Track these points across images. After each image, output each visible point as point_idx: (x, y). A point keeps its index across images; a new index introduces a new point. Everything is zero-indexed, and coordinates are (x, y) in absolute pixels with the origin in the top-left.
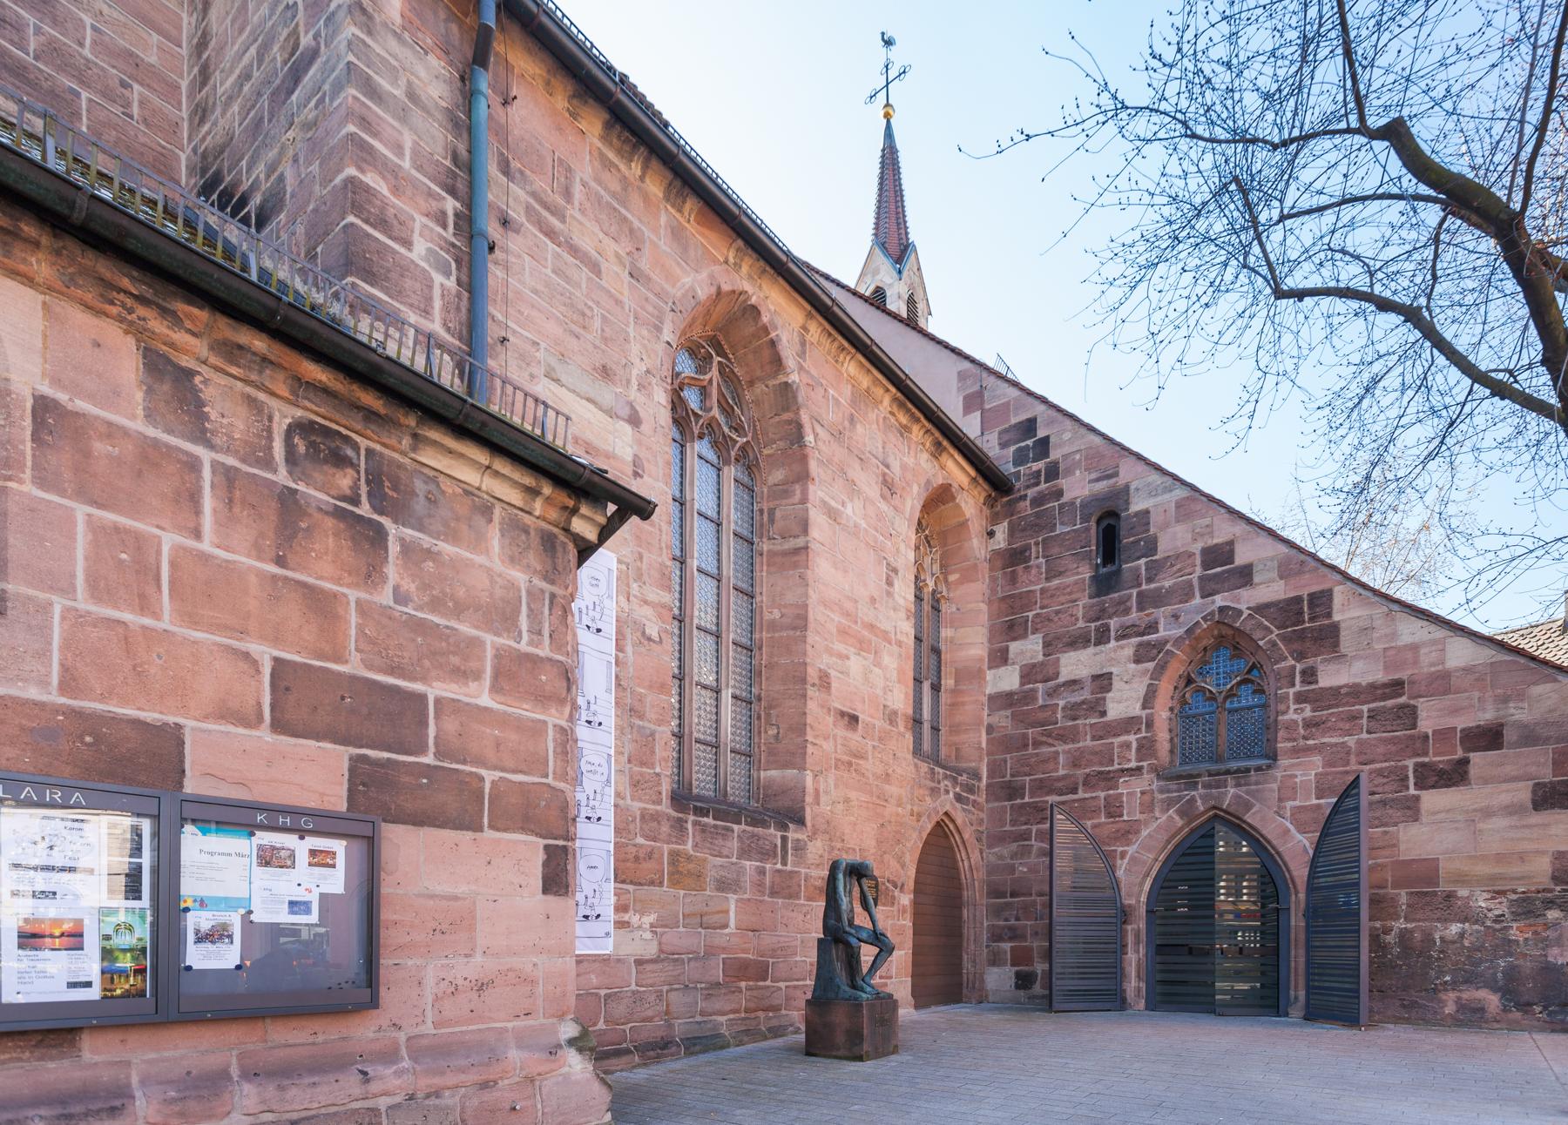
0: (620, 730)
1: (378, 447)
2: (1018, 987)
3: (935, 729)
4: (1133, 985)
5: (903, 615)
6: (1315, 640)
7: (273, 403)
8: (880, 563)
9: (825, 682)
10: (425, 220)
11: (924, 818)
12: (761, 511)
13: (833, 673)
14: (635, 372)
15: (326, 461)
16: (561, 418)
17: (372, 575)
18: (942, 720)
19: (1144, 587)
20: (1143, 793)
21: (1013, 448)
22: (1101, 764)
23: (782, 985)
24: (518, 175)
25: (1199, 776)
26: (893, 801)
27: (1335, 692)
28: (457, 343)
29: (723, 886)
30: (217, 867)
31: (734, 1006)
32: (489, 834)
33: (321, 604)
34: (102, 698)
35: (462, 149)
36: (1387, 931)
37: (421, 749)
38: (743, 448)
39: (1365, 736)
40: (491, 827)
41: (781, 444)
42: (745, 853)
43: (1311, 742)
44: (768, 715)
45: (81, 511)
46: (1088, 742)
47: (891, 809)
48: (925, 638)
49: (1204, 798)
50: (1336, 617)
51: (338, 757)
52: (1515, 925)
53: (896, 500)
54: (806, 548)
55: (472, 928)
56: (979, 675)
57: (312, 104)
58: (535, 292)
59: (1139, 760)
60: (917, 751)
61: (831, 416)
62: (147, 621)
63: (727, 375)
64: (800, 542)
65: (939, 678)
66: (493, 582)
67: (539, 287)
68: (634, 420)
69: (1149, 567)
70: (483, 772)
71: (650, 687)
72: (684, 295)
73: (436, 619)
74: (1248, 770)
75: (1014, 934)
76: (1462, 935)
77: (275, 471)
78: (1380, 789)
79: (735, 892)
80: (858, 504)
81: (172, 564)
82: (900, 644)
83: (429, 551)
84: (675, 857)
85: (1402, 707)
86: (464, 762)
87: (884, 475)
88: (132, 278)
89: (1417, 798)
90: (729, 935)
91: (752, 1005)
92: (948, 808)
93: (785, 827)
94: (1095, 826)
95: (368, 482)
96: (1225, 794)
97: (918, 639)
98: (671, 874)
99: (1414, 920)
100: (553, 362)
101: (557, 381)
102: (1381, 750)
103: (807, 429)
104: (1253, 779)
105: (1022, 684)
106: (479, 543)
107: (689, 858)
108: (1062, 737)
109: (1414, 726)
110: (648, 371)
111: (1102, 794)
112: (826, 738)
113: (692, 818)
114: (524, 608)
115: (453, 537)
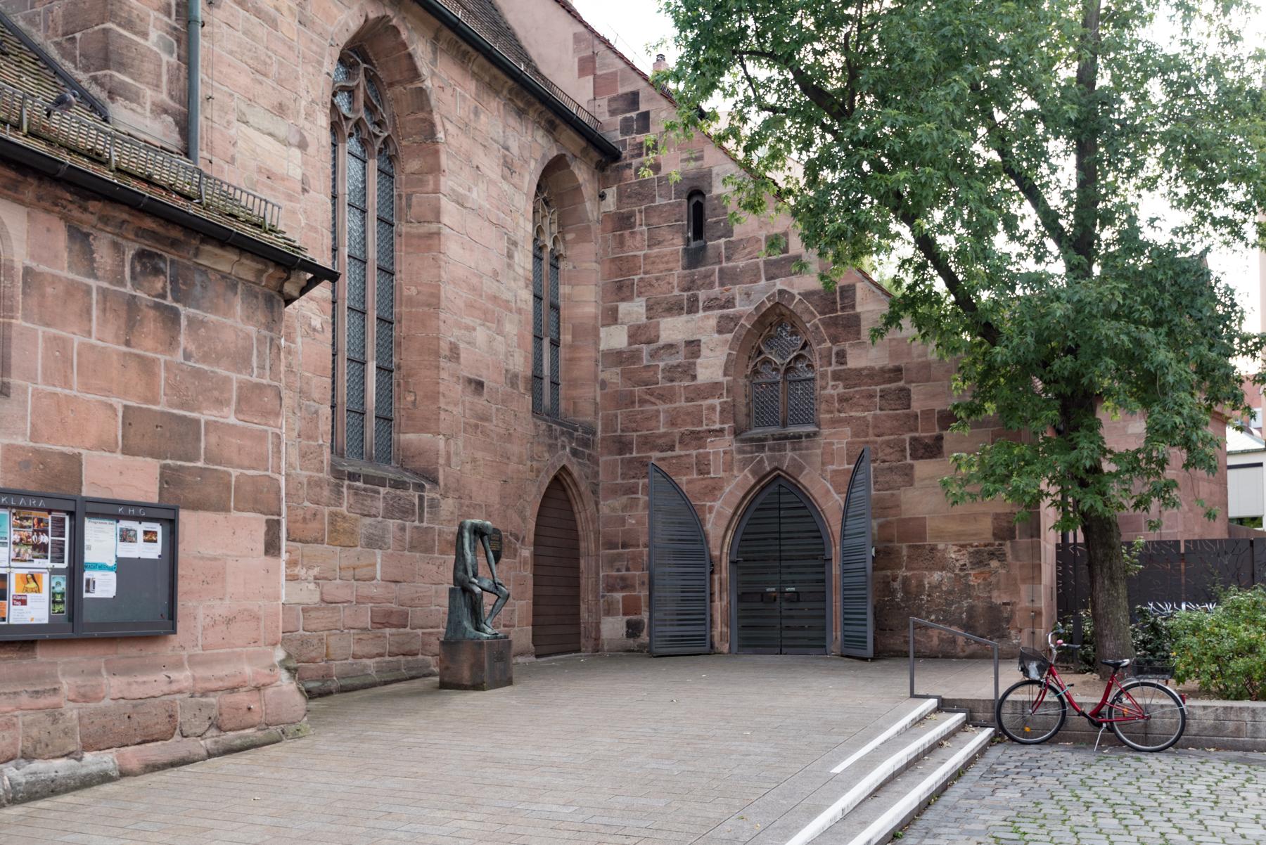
1: (176, 258)
2: (629, 635)
3: (555, 384)
4: (720, 629)
5: (522, 283)
6: (845, 326)
7: (124, 242)
12: (400, 196)
13: (462, 346)
14: (303, 103)
15: (150, 274)
16: (276, 209)
17: (172, 343)
18: (561, 375)
19: (724, 264)
20: (725, 453)
21: (620, 117)
22: (693, 425)
23: (419, 631)
25: (765, 439)
26: (515, 459)
27: (858, 372)
28: (177, 106)
29: (373, 542)
33: (146, 366)
37: (197, 459)
38: (386, 141)
39: (878, 412)
41: (418, 138)
42: (389, 514)
43: (842, 415)
44: (407, 383)
45: (41, 330)
47: (512, 466)
48: (544, 296)
49: (771, 459)
50: (859, 309)
52: (972, 572)
53: (516, 179)
54: (438, 234)
58: (231, 53)
59: (722, 422)
60: (537, 410)
63: (372, 79)
64: (433, 227)
65: (559, 333)
66: (237, 335)
67: (235, 49)
68: (303, 145)
69: (729, 246)
70: (230, 470)
72: (340, 31)
73: (205, 367)
74: (800, 437)
75: (625, 584)
77: (125, 286)
78: (888, 458)
80: (482, 186)
81: (79, 354)
82: (519, 311)
83: (202, 322)
84: (334, 515)
85: (902, 389)
86: (220, 464)
87: (505, 157)
88: (70, 192)
89: (912, 467)
91: (394, 649)
92: (565, 462)
94: (689, 482)
95: (171, 282)
96: (785, 456)
97: (537, 298)
98: (331, 532)
99: (912, 569)
100: (243, 107)
101: (246, 123)
102: (888, 424)
103: (439, 127)
104: (804, 444)
105: (630, 344)
108: (664, 397)
109: (909, 407)
110: (313, 101)
111: (694, 453)
112: (456, 404)
113: (346, 482)
114: (255, 351)
115: (214, 309)
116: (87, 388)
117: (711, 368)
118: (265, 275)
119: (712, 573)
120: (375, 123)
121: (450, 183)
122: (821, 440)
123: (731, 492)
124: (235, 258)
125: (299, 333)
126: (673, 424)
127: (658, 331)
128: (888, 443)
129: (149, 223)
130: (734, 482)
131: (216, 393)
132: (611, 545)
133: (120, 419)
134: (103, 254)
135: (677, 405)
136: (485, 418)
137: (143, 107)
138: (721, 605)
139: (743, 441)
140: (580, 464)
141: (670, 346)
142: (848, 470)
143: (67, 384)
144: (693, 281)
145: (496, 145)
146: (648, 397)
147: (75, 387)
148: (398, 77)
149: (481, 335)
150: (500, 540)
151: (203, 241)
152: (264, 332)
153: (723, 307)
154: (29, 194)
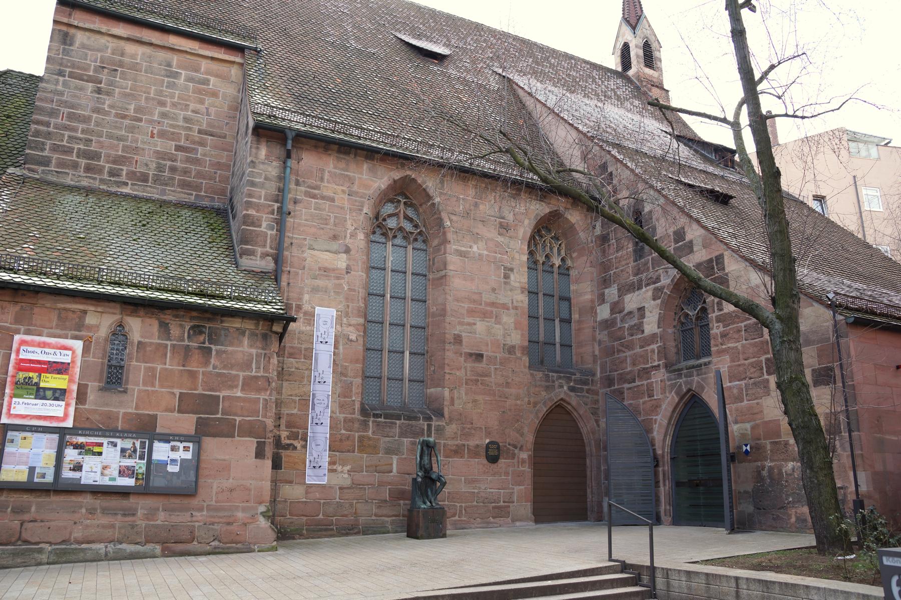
0: (335, 383)
8: (498, 268)
9: (458, 340)
13: (464, 334)
14: (349, 231)
17: (206, 363)
22: (644, 363)
25: (682, 370)
29: (389, 451)
30: (161, 452)
31: (395, 513)
32: (237, 438)
33: (193, 375)
35: (282, 185)
37: (217, 413)
39: (744, 342)
42: (403, 434)
45: (143, 365)
46: (638, 350)
47: (509, 403)
51: (193, 417)
53: (511, 233)
55: (229, 470)
56: (593, 311)
64: (443, 273)
65: (570, 314)
68: (347, 251)
71: (351, 362)
76: (793, 469)
78: (752, 376)
79: (396, 454)
80: (481, 244)
84: (361, 439)
90: (394, 476)
93: (429, 419)
94: (644, 403)
96: (693, 380)
101: (313, 249)
107: (369, 439)
112: (459, 369)
113: (372, 419)
115: (231, 344)
116: (162, 386)
117: (651, 326)
119: (657, 466)
122: (713, 367)
123: (666, 409)
126: (634, 365)
128: (752, 364)
129: (194, 314)
131: (229, 383)
134: (175, 331)
135: (635, 351)
136: (488, 375)
138: (664, 490)
139: (670, 372)
141: (630, 313)
143: (153, 385)
144: (639, 269)
146: (620, 348)
153: (654, 283)
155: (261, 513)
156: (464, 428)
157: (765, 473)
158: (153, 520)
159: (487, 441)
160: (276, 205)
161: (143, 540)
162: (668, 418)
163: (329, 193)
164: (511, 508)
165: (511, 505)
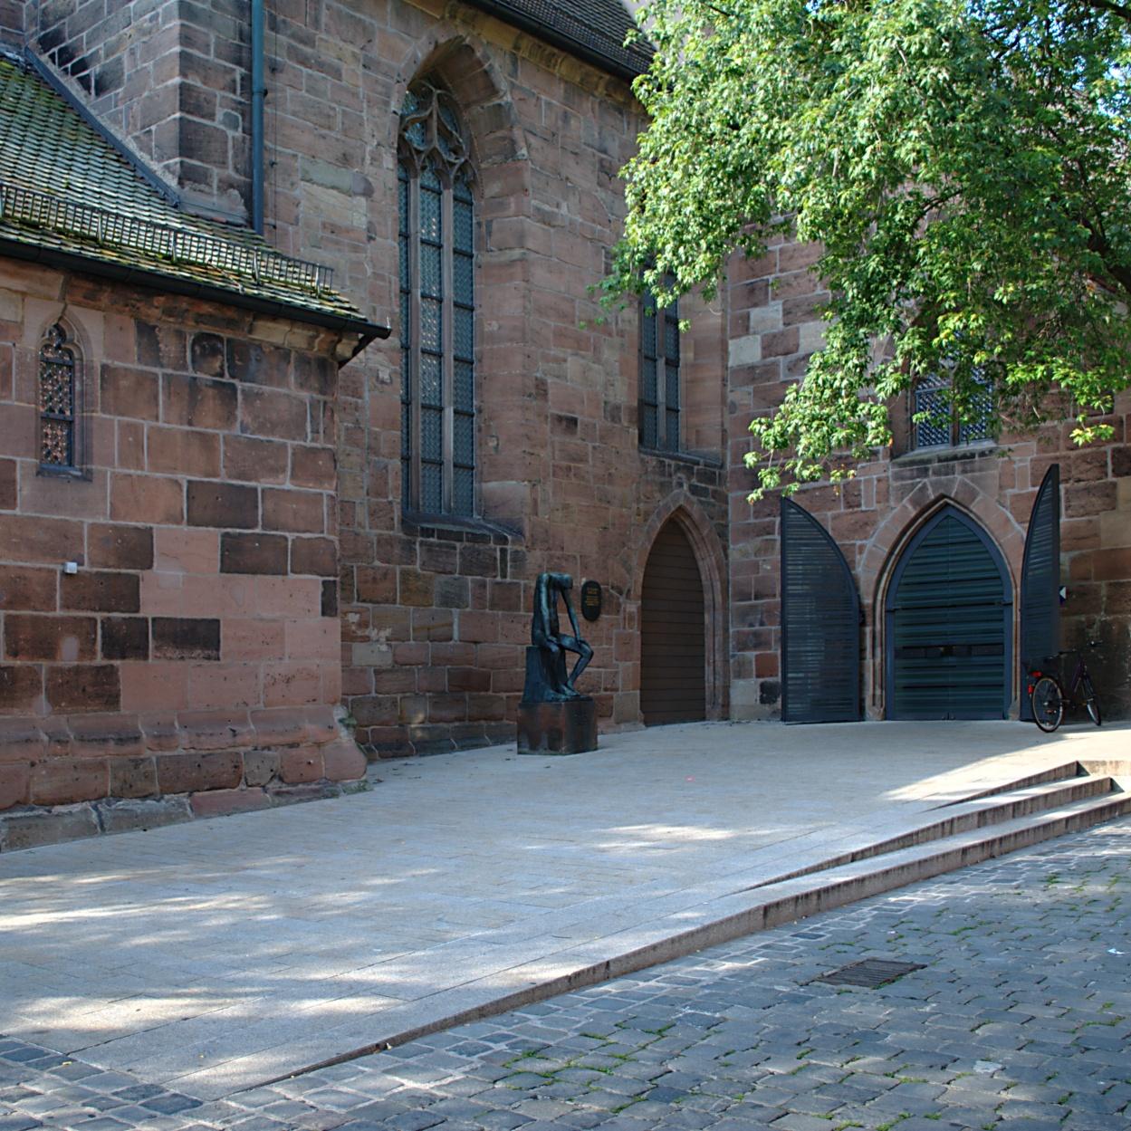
2: (763, 701)
3: (673, 411)
8: (597, 253)
10: (223, 93)
11: (653, 517)
14: (368, 148)
17: (229, 418)
23: (504, 695)
24: (282, 26)
28: (243, 178)
29: (449, 601)
32: (292, 576)
33: (207, 441)
34: (124, 519)
35: (245, 25)
36: (1090, 625)
37: (254, 526)
38: (462, 168)
40: (292, 571)
41: (498, 159)
42: (466, 570)
49: (934, 484)
57: (148, 16)
58: (294, 114)
61: (544, 121)
62: (139, 472)
65: (678, 351)
67: (297, 109)
68: (368, 192)
70: (287, 534)
73: (261, 437)
75: (759, 641)
78: (1083, 476)
81: (148, 438)
82: (621, 334)
84: (405, 574)
92: (682, 502)
94: (835, 518)
96: (952, 481)
98: (403, 592)
104: (977, 465)
105: (764, 357)
106: (282, 382)
107: (417, 576)
110: (379, 144)
115: (269, 380)
116: (155, 467)
118: (317, 341)
120: (450, 150)
121: (534, 202)
124: (287, 329)
125: (366, 388)
127: (798, 338)
129: (207, 308)
130: (890, 516)
131: (271, 462)
132: (744, 596)
133: (185, 494)
134: (168, 346)
136: (582, 459)
137: (209, 185)
138: (872, 663)
139: (904, 464)
140: (701, 502)
142: (1033, 493)
145: (590, 150)
147: (146, 467)
148: (475, 97)
149: (573, 366)
150: (599, 593)
151: (255, 318)
152: (317, 396)
154: (105, 298)
155: (341, 721)
156: (551, 557)
157: (1094, 632)
158: (170, 748)
159: (584, 580)
160: (239, 71)
161: (157, 788)
162: (891, 544)
163: (329, 56)
164: (615, 700)
165: (615, 694)
